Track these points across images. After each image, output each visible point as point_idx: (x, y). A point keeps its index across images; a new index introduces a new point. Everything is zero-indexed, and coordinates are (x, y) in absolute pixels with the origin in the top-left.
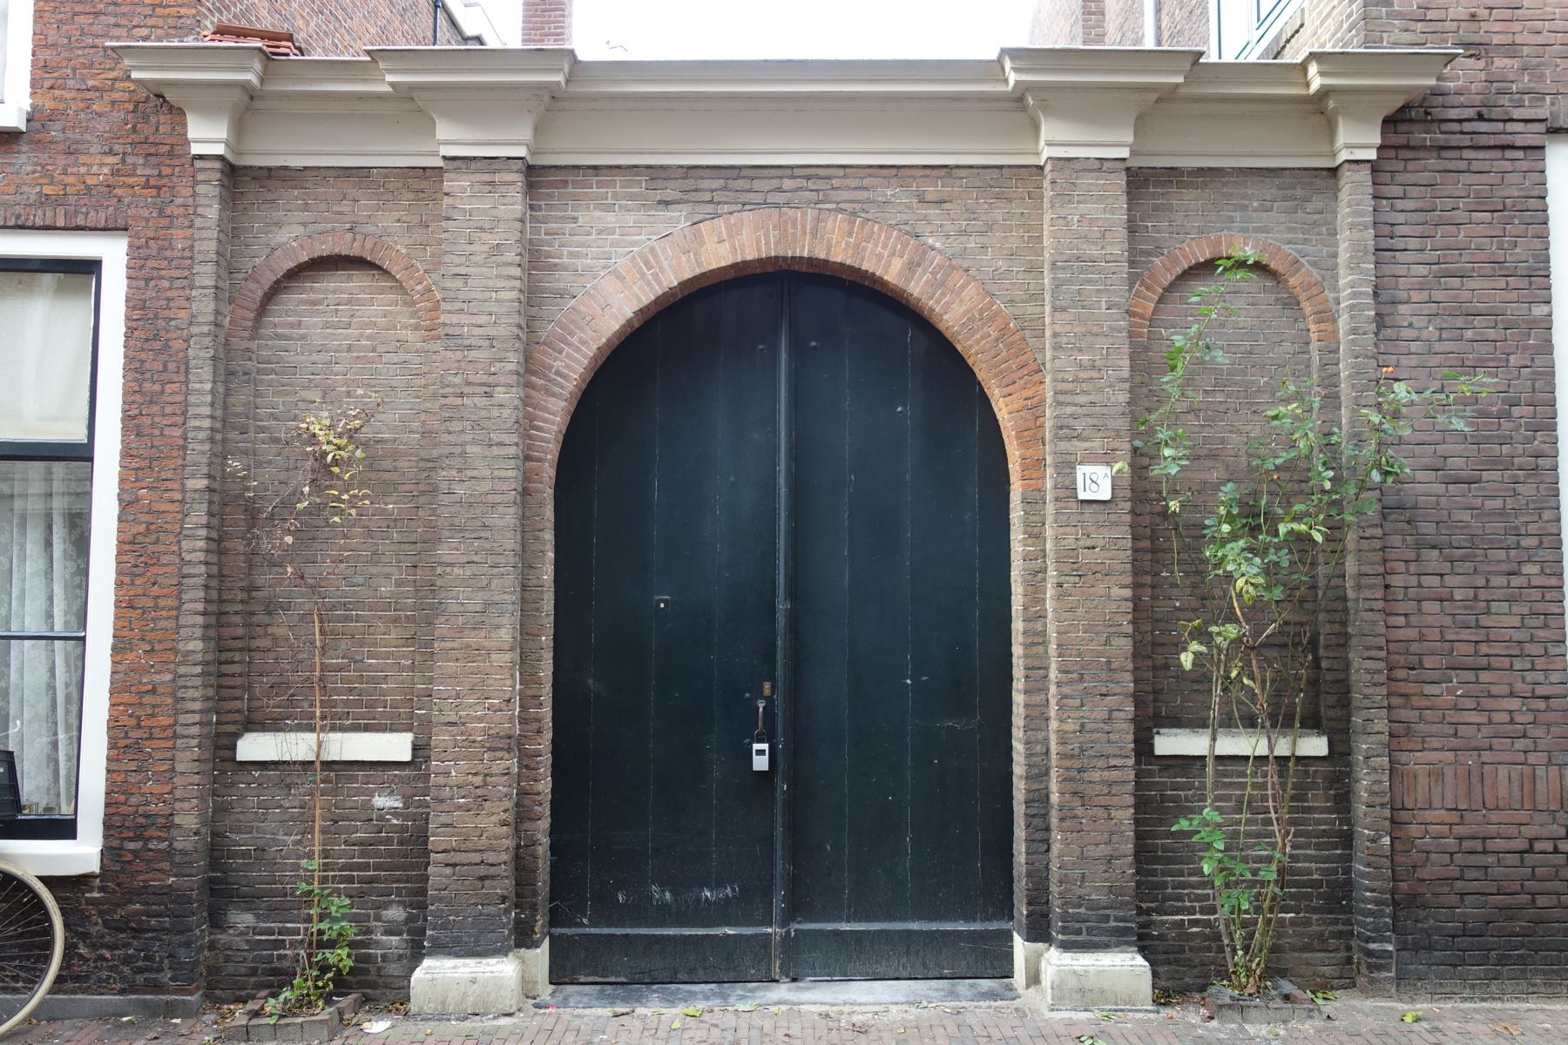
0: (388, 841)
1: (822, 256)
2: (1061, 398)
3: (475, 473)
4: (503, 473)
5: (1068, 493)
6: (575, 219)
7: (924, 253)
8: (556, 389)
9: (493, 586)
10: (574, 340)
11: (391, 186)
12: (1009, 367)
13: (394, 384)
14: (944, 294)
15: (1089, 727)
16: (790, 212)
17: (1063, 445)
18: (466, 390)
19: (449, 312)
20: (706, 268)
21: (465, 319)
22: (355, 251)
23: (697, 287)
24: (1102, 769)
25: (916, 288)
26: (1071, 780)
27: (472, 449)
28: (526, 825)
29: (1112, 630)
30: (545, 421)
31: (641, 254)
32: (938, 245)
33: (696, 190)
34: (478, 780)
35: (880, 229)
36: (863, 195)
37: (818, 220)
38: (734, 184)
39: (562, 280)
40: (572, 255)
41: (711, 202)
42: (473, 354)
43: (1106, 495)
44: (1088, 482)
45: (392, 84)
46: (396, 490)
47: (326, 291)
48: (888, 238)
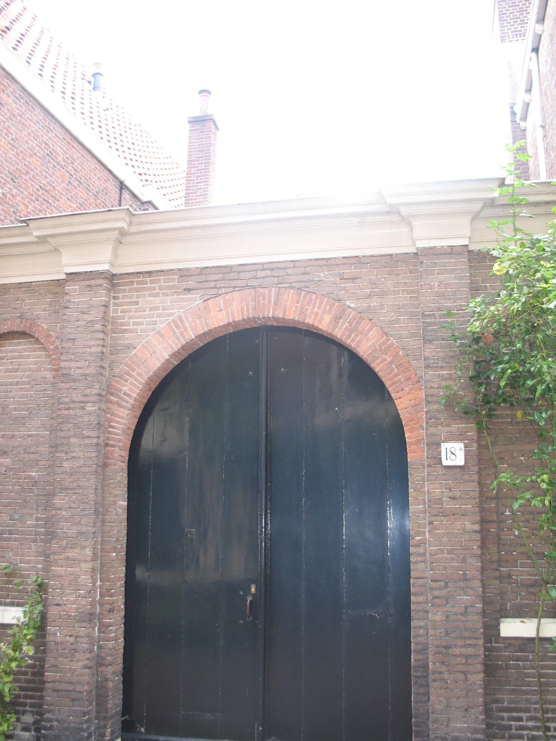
0: (25, 673)
1: (281, 316)
2: (430, 399)
3: (74, 454)
4: (89, 454)
5: (436, 461)
6: (137, 303)
7: (344, 310)
8: (124, 403)
9: (83, 522)
10: (134, 374)
11: (42, 292)
12: (399, 380)
13: (38, 403)
14: (357, 335)
15: (453, 617)
16: (261, 290)
17: (432, 430)
18: (72, 406)
19: (64, 361)
20: (211, 327)
21: (72, 364)
22: (22, 328)
23: (209, 339)
24: (462, 647)
25: (339, 333)
26: (439, 653)
27: (73, 440)
28: (102, 669)
29: (467, 552)
30: (117, 422)
31: (173, 321)
32: (352, 305)
33: (206, 281)
34: (72, 640)
35: (317, 297)
36: (306, 277)
37: (278, 294)
38: (227, 276)
39: (127, 339)
40: (136, 324)
41: (215, 287)
42: (77, 384)
43: (460, 461)
44: (449, 453)
45: (37, 237)
46: (37, 464)
47: (7, 352)
48: (321, 302)
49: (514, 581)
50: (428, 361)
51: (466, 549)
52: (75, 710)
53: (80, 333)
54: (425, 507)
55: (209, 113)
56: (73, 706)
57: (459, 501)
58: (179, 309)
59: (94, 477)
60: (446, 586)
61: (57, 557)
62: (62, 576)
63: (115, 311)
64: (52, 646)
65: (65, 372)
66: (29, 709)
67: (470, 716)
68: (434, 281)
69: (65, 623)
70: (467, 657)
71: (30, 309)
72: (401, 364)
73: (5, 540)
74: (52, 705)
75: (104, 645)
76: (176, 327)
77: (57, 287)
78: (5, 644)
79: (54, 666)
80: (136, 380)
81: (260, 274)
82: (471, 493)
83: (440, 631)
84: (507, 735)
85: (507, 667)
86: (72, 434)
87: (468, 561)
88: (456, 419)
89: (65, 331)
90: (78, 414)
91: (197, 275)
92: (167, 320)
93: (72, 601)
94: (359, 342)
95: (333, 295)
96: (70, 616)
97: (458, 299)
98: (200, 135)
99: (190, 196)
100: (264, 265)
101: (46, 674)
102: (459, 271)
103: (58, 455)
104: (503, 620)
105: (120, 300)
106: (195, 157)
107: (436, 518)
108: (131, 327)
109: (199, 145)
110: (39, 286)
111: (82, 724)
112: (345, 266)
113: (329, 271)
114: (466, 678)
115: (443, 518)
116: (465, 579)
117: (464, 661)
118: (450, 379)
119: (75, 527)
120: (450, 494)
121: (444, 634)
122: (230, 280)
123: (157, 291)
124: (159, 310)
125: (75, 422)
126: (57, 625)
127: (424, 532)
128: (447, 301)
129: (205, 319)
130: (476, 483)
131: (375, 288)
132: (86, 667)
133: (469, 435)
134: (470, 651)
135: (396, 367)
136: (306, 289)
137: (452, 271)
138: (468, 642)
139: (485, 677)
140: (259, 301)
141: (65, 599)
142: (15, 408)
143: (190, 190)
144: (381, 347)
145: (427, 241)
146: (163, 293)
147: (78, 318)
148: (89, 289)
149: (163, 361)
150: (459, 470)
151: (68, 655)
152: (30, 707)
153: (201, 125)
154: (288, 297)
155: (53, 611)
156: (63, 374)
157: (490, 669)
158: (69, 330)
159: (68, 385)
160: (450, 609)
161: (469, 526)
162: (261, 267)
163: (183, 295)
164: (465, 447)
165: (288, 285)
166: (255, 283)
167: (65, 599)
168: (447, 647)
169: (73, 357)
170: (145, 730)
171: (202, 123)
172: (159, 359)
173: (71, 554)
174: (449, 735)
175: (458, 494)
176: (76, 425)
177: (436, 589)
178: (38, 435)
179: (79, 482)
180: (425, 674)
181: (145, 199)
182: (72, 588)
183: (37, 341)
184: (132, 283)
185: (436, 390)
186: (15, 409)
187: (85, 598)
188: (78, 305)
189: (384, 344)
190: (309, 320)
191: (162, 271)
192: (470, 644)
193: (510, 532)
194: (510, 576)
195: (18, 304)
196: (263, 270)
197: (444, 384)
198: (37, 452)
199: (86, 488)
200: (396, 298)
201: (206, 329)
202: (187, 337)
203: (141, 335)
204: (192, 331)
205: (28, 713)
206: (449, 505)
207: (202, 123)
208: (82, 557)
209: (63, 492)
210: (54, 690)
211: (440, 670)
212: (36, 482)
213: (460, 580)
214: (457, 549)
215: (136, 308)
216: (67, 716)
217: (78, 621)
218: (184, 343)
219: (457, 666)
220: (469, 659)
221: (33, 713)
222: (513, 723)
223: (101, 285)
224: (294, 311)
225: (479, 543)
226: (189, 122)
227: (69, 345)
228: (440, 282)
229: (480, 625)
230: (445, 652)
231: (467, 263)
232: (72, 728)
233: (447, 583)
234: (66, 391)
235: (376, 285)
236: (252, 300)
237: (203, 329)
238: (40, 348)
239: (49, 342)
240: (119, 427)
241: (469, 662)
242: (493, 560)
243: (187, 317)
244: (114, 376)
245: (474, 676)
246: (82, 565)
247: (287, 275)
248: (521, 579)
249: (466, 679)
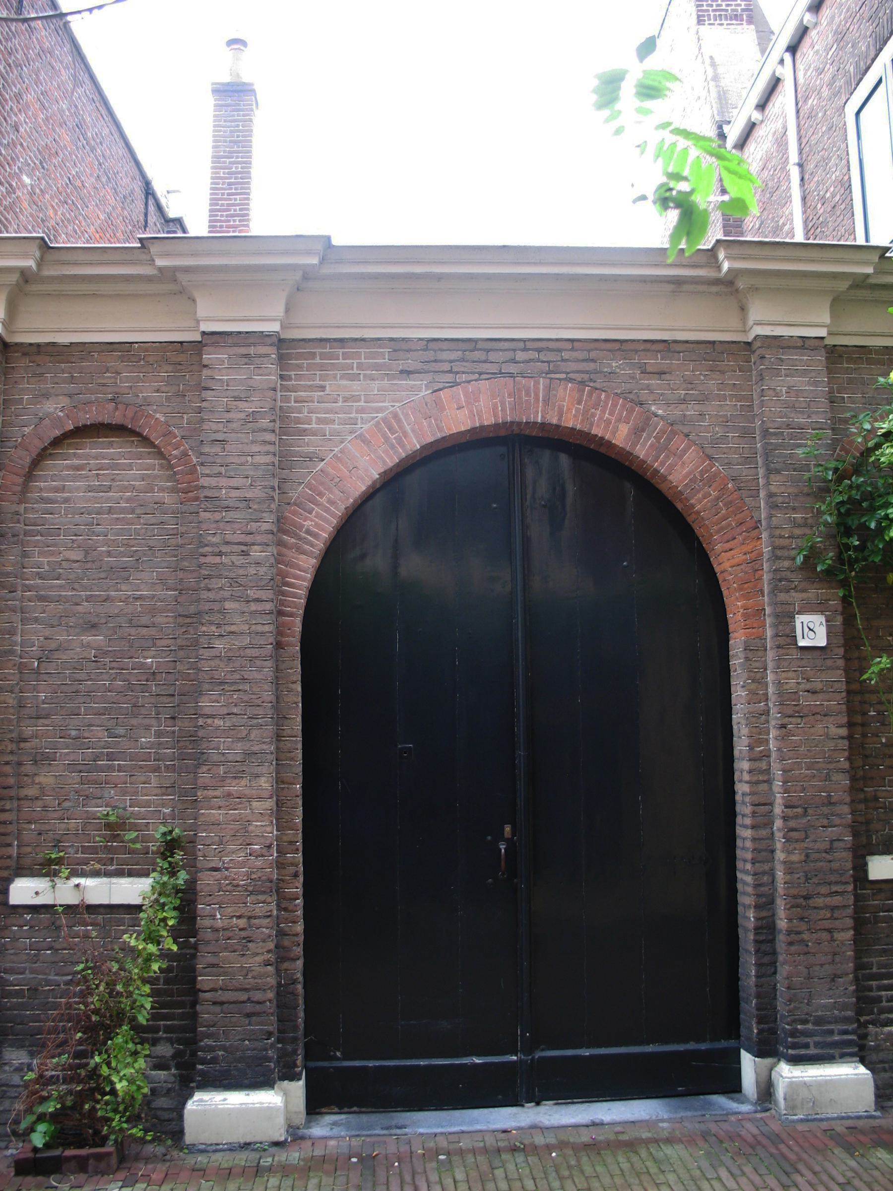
1: (555, 421)
2: (779, 553)
3: (233, 628)
4: (260, 628)
6: (323, 388)
7: (648, 419)
9: (252, 737)
10: (323, 501)
11: (151, 359)
13: (151, 543)
16: (524, 381)
17: (782, 597)
18: (225, 549)
19: (208, 476)
20: (447, 432)
21: (223, 482)
24: (825, 896)
26: (797, 906)
27: (228, 605)
28: (286, 965)
29: (831, 766)
31: (385, 420)
32: (660, 412)
33: (435, 361)
34: (242, 923)
35: (607, 397)
36: (591, 366)
37: (549, 389)
39: (309, 445)
40: (320, 421)
41: (450, 372)
42: (232, 515)
44: (806, 630)
45: (160, 269)
46: (154, 645)
47: (87, 457)
48: (614, 405)
49: (881, 805)
50: (774, 499)
51: (830, 762)
52: (253, 1030)
53: (233, 431)
54: (767, 705)
55: (245, 79)
56: (250, 1024)
57: (821, 696)
58: (393, 402)
59: (269, 664)
60: (805, 813)
61: (211, 793)
62: (219, 824)
63: (286, 399)
64: (209, 935)
65: (210, 495)
66: (165, 1035)
67: (837, 988)
68: (781, 384)
69: (229, 897)
70: (833, 909)
71: (131, 387)
72: (731, 502)
73: (101, 769)
74: (212, 1026)
75: (287, 929)
76: (389, 430)
77: (187, 356)
78: (131, 935)
79: (213, 966)
80: (327, 510)
81: (520, 356)
82: (836, 686)
83: (798, 876)
84: (875, 1010)
85: (877, 920)
86: (227, 594)
87: (833, 778)
88: (814, 582)
89: (207, 427)
90: (237, 563)
91: (421, 350)
92: (373, 418)
93: (238, 862)
94: (672, 467)
95: (631, 396)
96: (238, 886)
97: (813, 413)
98: (233, 116)
99: (217, 216)
100: (527, 343)
101: (199, 978)
102: (813, 374)
103: (204, 629)
104: (868, 858)
105: (293, 382)
106: (225, 151)
107: (790, 719)
108: (314, 426)
109: (231, 132)
110: (147, 350)
111: (266, 1050)
112: (648, 354)
113: (625, 359)
114: (832, 937)
115: (799, 720)
116: (830, 803)
117: (829, 915)
118: (805, 525)
119: (239, 745)
120: (808, 686)
121: (803, 880)
122: (474, 362)
123: (355, 371)
124: (359, 401)
125: (232, 575)
126: (215, 901)
127: (767, 741)
128: (800, 415)
129: (436, 420)
130: (842, 672)
131: (692, 389)
132: (267, 963)
133: (831, 605)
134: (836, 900)
135: (725, 505)
136: (592, 384)
137: (805, 373)
138: (834, 888)
139: (854, 935)
140: (520, 398)
141: (227, 859)
142: (109, 552)
143: (217, 205)
144: (702, 476)
145: (772, 328)
146: (365, 375)
147: (229, 407)
148: (246, 360)
149: (370, 483)
150: (819, 652)
151: (236, 947)
152: (165, 1032)
153: (235, 98)
154: (565, 394)
155: (206, 881)
156: (206, 497)
157: (861, 924)
158: (214, 427)
159: (217, 516)
160: (811, 845)
161: (834, 731)
162: (521, 345)
163: (399, 379)
164: (827, 621)
165: (563, 376)
166: (512, 368)
167: (227, 859)
168: (806, 898)
169: (223, 470)
170: (342, 1054)
171: (234, 96)
172: (362, 479)
173: (234, 788)
174: (811, 1016)
175: (819, 686)
176: (234, 582)
177: (792, 818)
178: (154, 596)
179: (243, 673)
180: (770, 937)
181: (172, 214)
182: (238, 842)
183: (146, 441)
184: (313, 355)
185: (787, 540)
186: (109, 553)
187: (263, 856)
188: (227, 385)
189: (707, 471)
190: (597, 431)
191: (363, 340)
192: (836, 892)
193: (875, 739)
194: (876, 799)
195: (108, 377)
196: (525, 350)
197: (797, 532)
198: (154, 625)
199: (256, 682)
200: (721, 405)
201: (439, 435)
202: (408, 447)
203: (330, 440)
204: (416, 438)
205: (162, 1042)
206: (807, 701)
207: (234, 96)
208: (254, 792)
209: (216, 689)
210: (215, 1003)
211: (799, 929)
212: (154, 673)
213: (823, 805)
214: (818, 762)
215: (321, 396)
216: (240, 1040)
217: (251, 893)
218: (404, 455)
219: (820, 922)
220: (836, 911)
221: (171, 1041)
222: (883, 993)
223: (267, 355)
224: (575, 416)
225: (846, 754)
226: (215, 91)
227: (217, 449)
228: (789, 387)
229: (849, 865)
230: (804, 904)
231: (824, 362)
232: (249, 1057)
233: (805, 809)
234: (214, 525)
235: (693, 386)
236: (510, 396)
237: (433, 435)
238: (149, 453)
239: (169, 444)
240: (302, 585)
241: (835, 915)
242: (858, 776)
243: (406, 416)
244: (289, 504)
245: (842, 934)
246: (255, 804)
247: (563, 360)
248: (889, 802)
249: (833, 940)
